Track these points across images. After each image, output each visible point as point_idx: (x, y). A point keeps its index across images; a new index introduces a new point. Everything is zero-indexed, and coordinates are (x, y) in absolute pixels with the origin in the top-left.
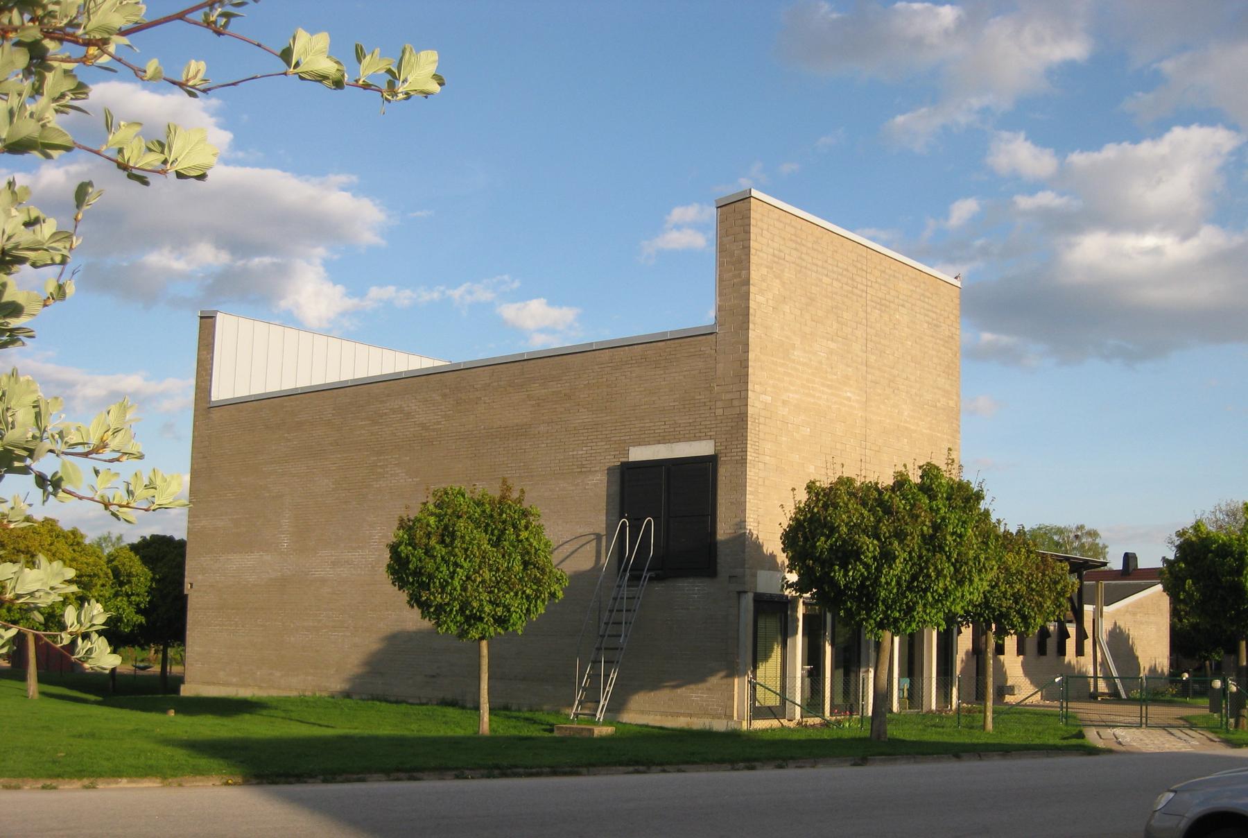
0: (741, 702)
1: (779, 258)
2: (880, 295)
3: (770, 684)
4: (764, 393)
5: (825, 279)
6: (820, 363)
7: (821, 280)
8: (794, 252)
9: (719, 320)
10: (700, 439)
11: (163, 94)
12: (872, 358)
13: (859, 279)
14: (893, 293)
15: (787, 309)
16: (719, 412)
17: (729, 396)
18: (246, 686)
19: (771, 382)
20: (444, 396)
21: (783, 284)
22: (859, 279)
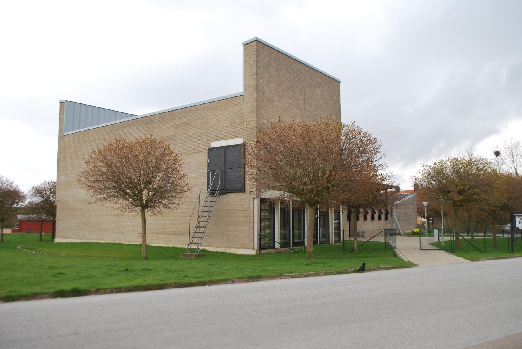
0: (332, 217)
1: (268, 65)
2: (309, 82)
3: (267, 235)
4: (263, 118)
5: (287, 75)
6: (286, 107)
7: (286, 75)
8: (275, 64)
9: (245, 91)
10: (237, 137)
11: (472, 260)
12: (307, 107)
13: (301, 76)
14: (315, 82)
15: (272, 85)
16: (245, 126)
17: (248, 120)
18: (76, 238)
19: (266, 114)
20: (144, 126)
21: (270, 76)
22: (301, 76)
